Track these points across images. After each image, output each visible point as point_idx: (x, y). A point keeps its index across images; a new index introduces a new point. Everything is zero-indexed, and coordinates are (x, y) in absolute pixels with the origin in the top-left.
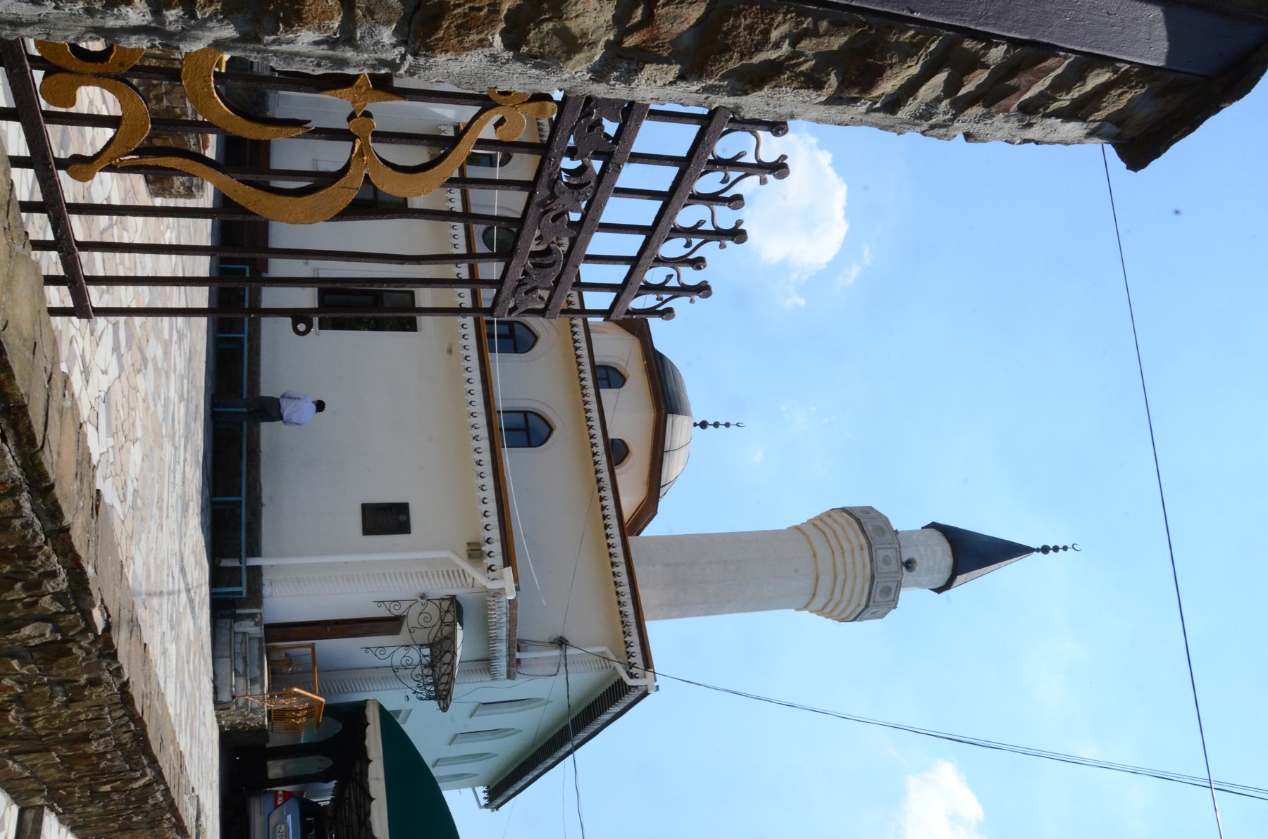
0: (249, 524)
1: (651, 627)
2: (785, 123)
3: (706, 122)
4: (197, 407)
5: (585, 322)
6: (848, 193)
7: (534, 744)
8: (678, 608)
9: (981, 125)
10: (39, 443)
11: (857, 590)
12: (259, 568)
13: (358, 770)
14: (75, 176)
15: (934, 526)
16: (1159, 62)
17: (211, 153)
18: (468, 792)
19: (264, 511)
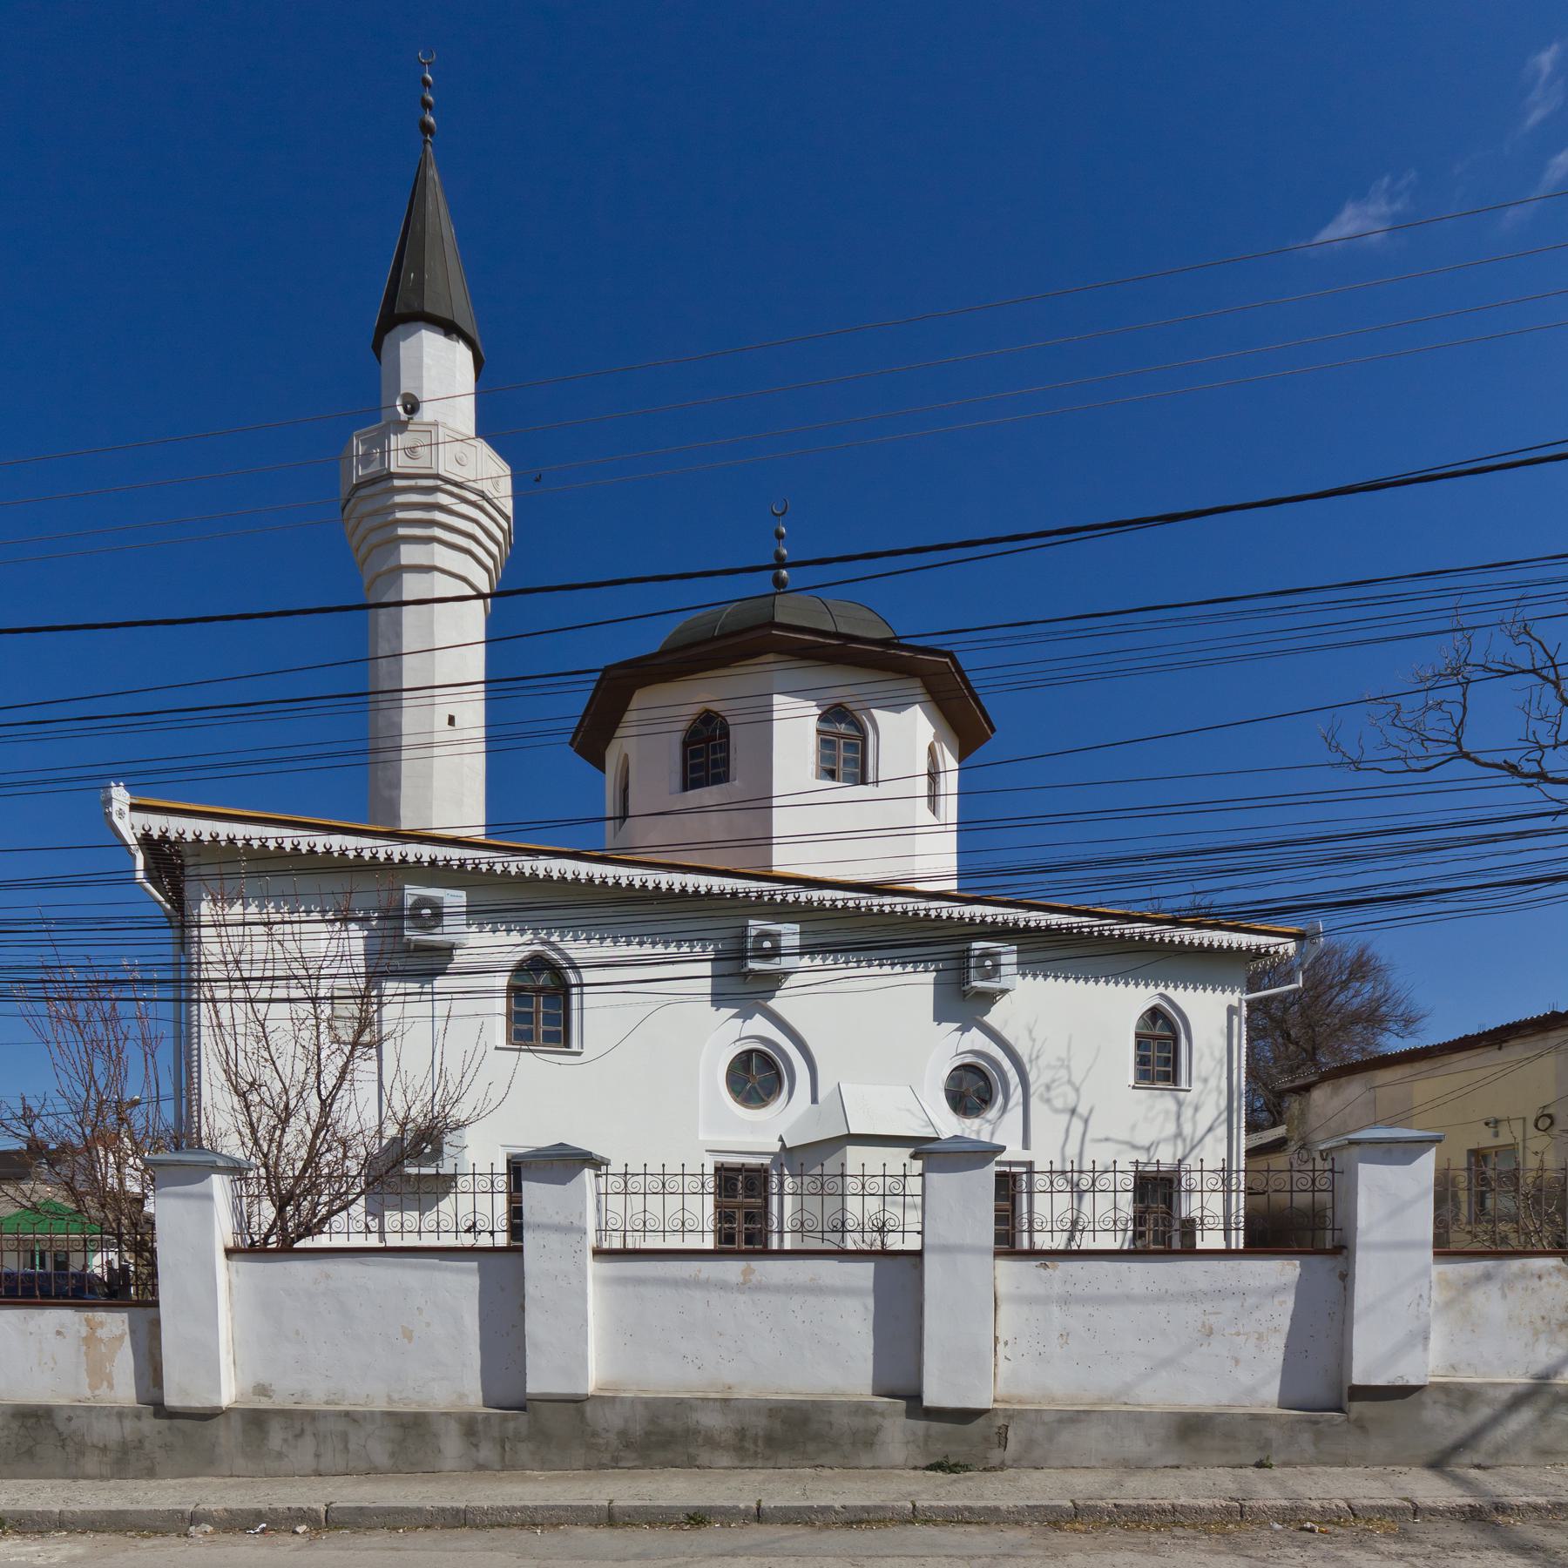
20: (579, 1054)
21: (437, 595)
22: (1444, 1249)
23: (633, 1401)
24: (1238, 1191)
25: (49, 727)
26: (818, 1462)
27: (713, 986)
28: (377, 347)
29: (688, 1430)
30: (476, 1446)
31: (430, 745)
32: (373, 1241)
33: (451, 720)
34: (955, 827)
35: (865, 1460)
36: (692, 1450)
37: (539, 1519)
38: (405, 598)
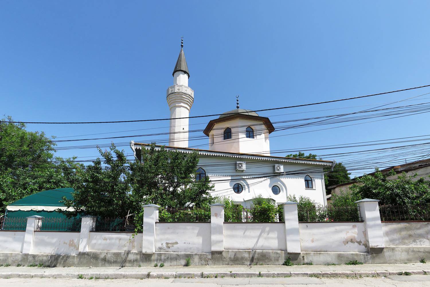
0: (238, 250)
1: (241, 152)
2: (159, 221)
3: (178, 68)
4: (105, 239)
5: (254, 237)
6: (278, 241)
7: (389, 223)
8: (367, 210)
9: (229, 254)
10: (330, 164)
11: (412, 150)
12: (23, 228)
13: (322, 267)
14: (386, 216)
15: (173, 75)
16: (212, 249)
17: (278, 221)
18: (320, 180)
19: (290, 252)
20: (315, 190)
21: (176, 118)
22: (140, 231)
23: (293, 264)
24: (406, 162)
25: (322, 122)
26: (268, 264)
27: (189, 135)
28: (173, 75)
29: (242, 257)
30: (201, 260)
31: (270, 153)
32: (300, 152)
33: (183, 129)
34: (187, 135)
35: (277, 263)
36: (243, 261)
37: (10, 261)
38: (176, 131)
